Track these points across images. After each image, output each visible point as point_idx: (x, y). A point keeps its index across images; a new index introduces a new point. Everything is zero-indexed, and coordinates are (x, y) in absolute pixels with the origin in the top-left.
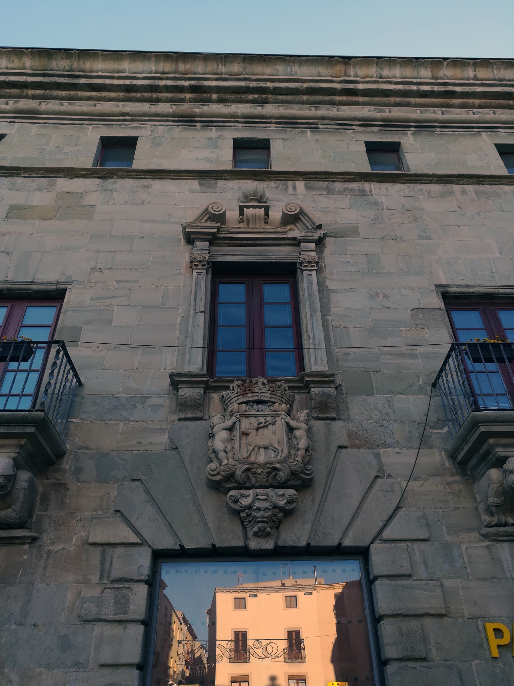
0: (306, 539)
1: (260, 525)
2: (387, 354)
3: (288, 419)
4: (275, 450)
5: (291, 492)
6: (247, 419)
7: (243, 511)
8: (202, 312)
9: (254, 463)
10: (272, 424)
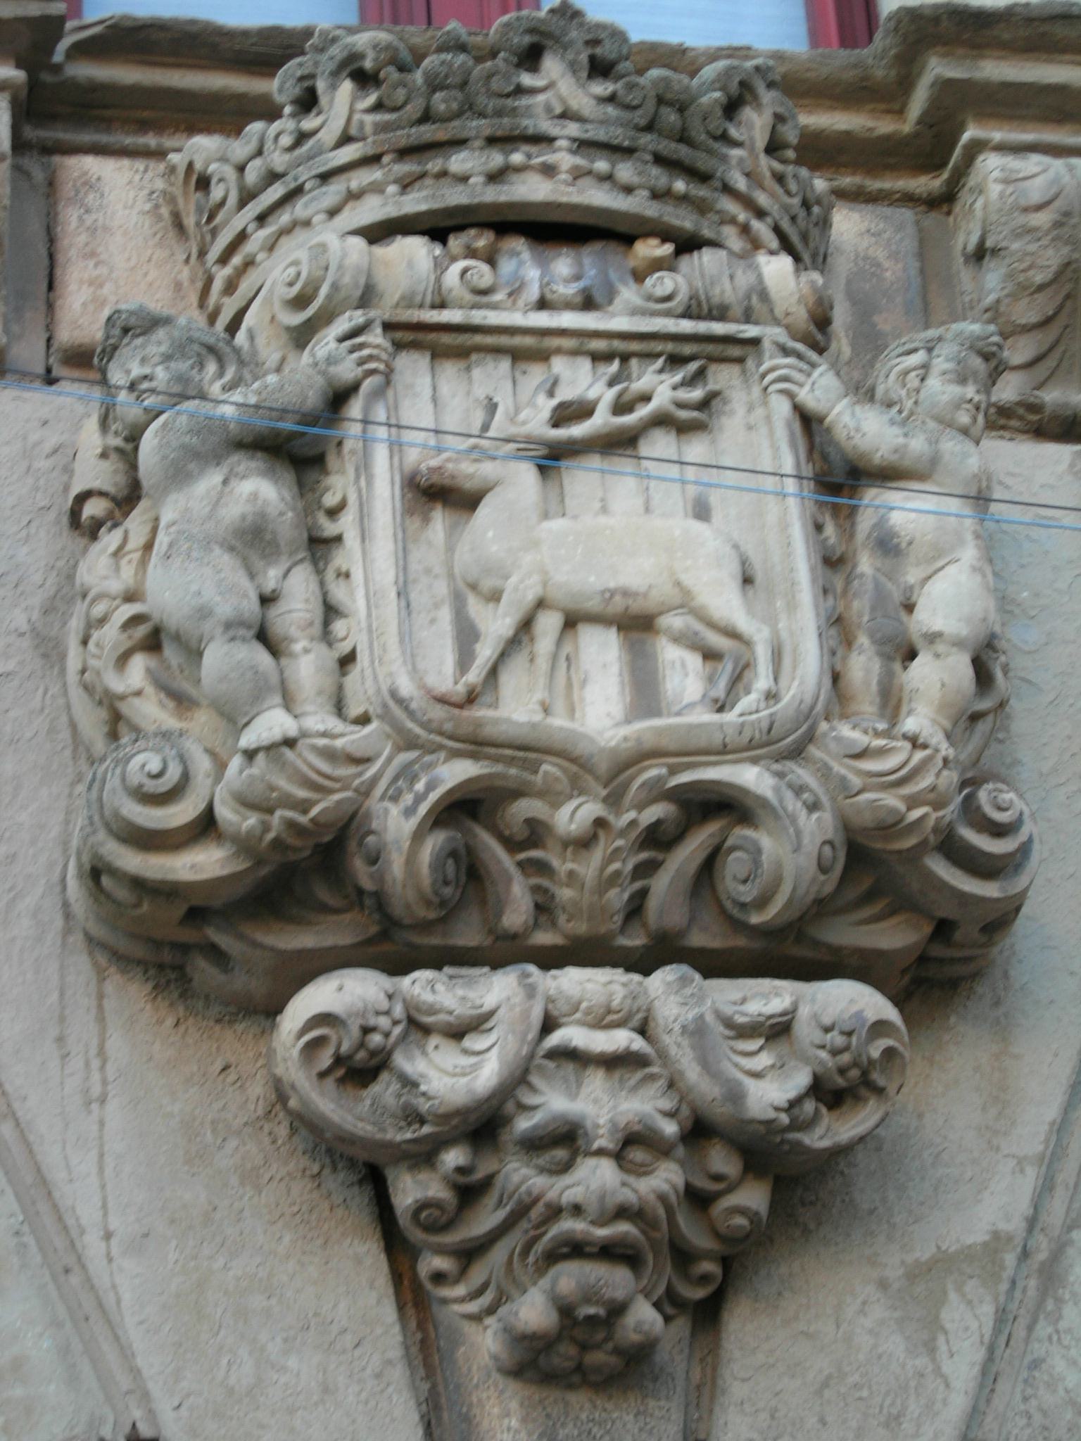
1: (570, 1277)
4: (716, 640)
5: (849, 1000)
6: (449, 369)
7: (423, 1156)
9: (528, 750)
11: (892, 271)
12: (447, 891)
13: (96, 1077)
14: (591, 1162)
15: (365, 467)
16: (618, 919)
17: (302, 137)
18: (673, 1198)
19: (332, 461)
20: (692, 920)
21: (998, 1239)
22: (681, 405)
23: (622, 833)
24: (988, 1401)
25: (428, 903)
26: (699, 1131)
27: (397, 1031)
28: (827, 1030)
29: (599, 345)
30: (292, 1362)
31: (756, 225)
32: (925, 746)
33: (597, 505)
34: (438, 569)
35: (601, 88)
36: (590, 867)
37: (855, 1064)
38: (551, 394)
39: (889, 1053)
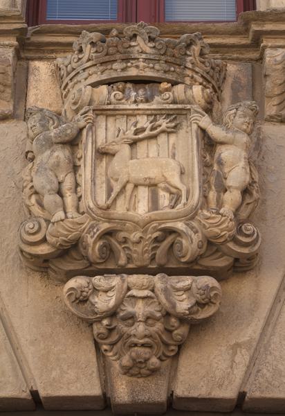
3: (205, 122)
4: (173, 190)
6: (111, 120)
7: (99, 321)
9: (123, 220)
10: (169, 133)
11: (244, 81)
12: (104, 256)
15: (86, 148)
19: (80, 145)
22: (168, 128)
23: (147, 240)
24: (248, 380)
26: (167, 315)
28: (199, 289)
29: (149, 112)
31: (195, 76)
32: (225, 216)
33: (146, 155)
34: (103, 174)
35: (152, 45)
36: (139, 248)
38: (135, 126)
39: (216, 294)
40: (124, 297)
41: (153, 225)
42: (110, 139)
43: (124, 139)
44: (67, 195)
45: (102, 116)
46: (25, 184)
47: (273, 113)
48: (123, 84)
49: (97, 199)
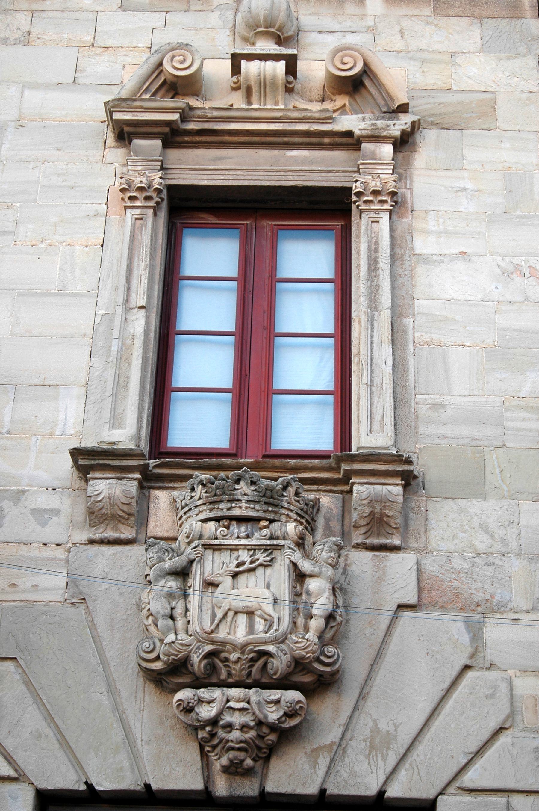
0: (319, 780)
2: (522, 408)
3: (297, 556)
5: (294, 695)
6: (217, 553)
7: (203, 728)
8: (142, 307)
9: (224, 643)
10: (266, 566)
12: (208, 672)
13: (142, 705)
14: (235, 731)
16: (245, 677)
17: (192, 497)
18: (253, 738)
19: (190, 574)
20: (262, 677)
21: (333, 743)
22: (265, 561)
23: (244, 660)
25: (204, 675)
27: (196, 702)
28: (287, 703)
29: (249, 547)
30: (177, 769)
34: (209, 601)
35: (253, 488)
36: (238, 667)
37: (293, 710)
38: (237, 560)
39: (301, 707)
40: (224, 708)
41: (249, 648)
42: (216, 572)
43: (226, 571)
44: (178, 619)
45: (209, 550)
46: (143, 606)
47: (359, 541)
48: (228, 521)
49: (203, 624)
